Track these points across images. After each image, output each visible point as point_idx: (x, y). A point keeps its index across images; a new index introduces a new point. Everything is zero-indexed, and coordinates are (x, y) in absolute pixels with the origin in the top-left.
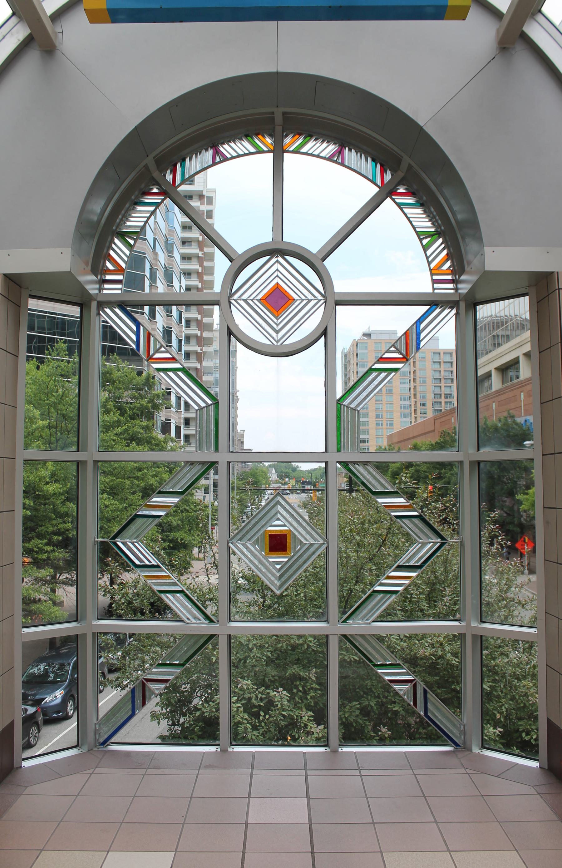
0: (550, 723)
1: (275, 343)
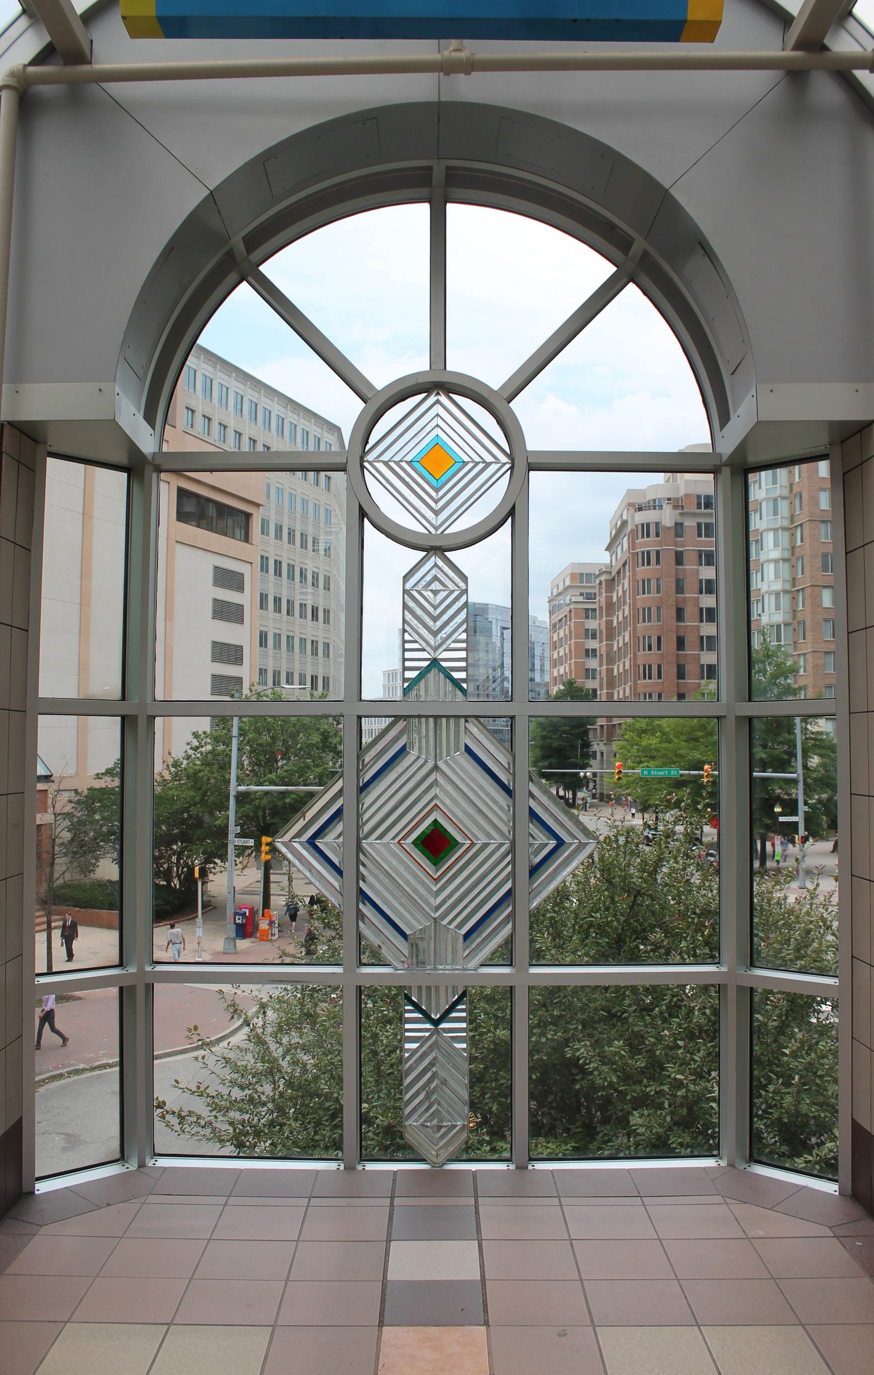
0: (857, 1129)
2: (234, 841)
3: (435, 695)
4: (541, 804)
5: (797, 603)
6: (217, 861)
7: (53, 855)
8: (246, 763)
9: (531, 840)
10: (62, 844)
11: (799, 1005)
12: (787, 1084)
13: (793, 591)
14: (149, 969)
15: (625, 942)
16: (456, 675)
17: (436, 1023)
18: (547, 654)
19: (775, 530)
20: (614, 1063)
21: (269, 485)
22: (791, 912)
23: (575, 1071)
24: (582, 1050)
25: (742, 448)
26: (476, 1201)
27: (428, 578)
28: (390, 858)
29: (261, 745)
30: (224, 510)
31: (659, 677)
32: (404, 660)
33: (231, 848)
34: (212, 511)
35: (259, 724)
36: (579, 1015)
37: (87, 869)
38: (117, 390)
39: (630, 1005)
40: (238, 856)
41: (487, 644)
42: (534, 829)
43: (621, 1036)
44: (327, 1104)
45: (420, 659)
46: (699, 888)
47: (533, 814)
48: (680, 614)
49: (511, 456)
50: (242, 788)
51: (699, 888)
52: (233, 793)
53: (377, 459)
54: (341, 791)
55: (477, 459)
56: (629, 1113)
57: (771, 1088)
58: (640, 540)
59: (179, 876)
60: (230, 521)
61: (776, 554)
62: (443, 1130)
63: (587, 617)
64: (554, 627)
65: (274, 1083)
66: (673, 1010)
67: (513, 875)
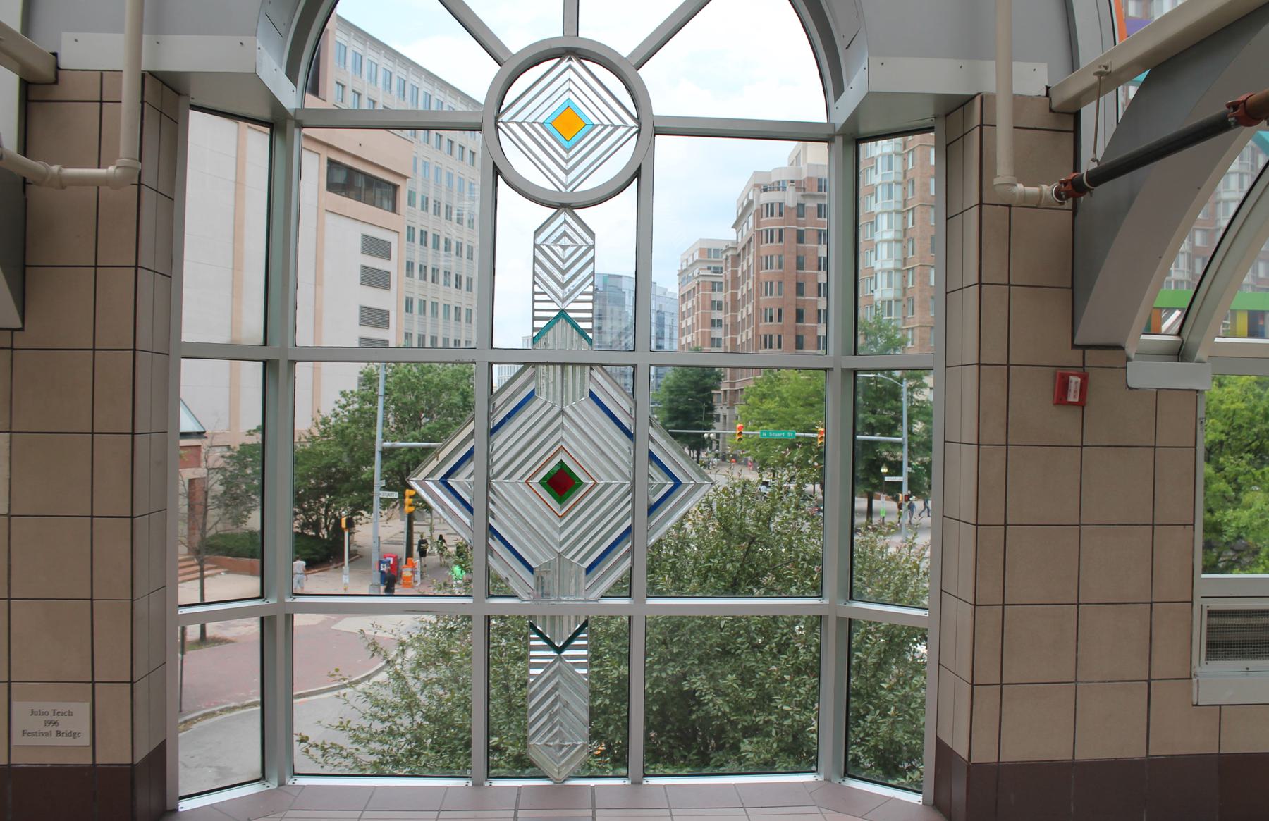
1: (563, 189)
2: (379, 494)
3: (562, 342)
4: (660, 447)
5: (907, 281)
6: (364, 512)
7: (206, 506)
8: (391, 420)
9: (650, 481)
10: (214, 497)
11: (898, 639)
12: (884, 714)
13: (904, 270)
14: (288, 600)
15: (740, 585)
16: (583, 325)
17: (559, 650)
18: (676, 324)
19: (889, 213)
20: (727, 695)
21: (416, 159)
22: (892, 559)
23: (691, 703)
24: (698, 683)
25: (854, 118)
26: (594, 813)
27: (558, 234)
28: (517, 496)
29: (405, 404)
30: (372, 182)
31: (779, 346)
32: (534, 310)
33: (376, 501)
34: (360, 182)
35: (405, 385)
36: (696, 652)
37: (239, 520)
38: (259, 44)
39: (743, 643)
40: (383, 508)
41: (620, 313)
42: (653, 470)
43: (734, 671)
44: (461, 735)
45: (549, 309)
46: (809, 536)
47: (652, 456)
48: (800, 289)
49: (638, 121)
50: (388, 444)
51: (809, 536)
52: (378, 448)
53: (511, 120)
54: (473, 433)
55: (606, 122)
56: (740, 741)
57: (869, 718)
58: (764, 219)
59: (327, 527)
60: (378, 191)
61: (889, 235)
62: (565, 750)
63: (714, 290)
64: (683, 298)
65: (412, 716)
66: (783, 647)
67: (632, 513)
